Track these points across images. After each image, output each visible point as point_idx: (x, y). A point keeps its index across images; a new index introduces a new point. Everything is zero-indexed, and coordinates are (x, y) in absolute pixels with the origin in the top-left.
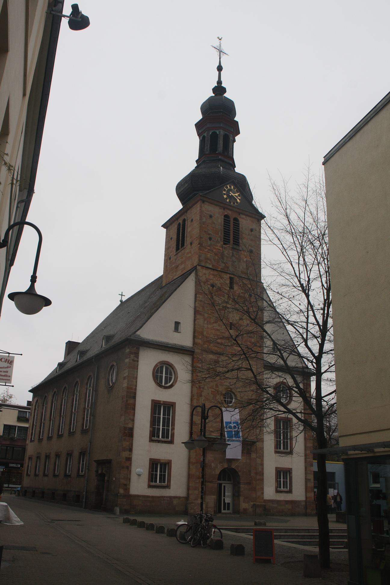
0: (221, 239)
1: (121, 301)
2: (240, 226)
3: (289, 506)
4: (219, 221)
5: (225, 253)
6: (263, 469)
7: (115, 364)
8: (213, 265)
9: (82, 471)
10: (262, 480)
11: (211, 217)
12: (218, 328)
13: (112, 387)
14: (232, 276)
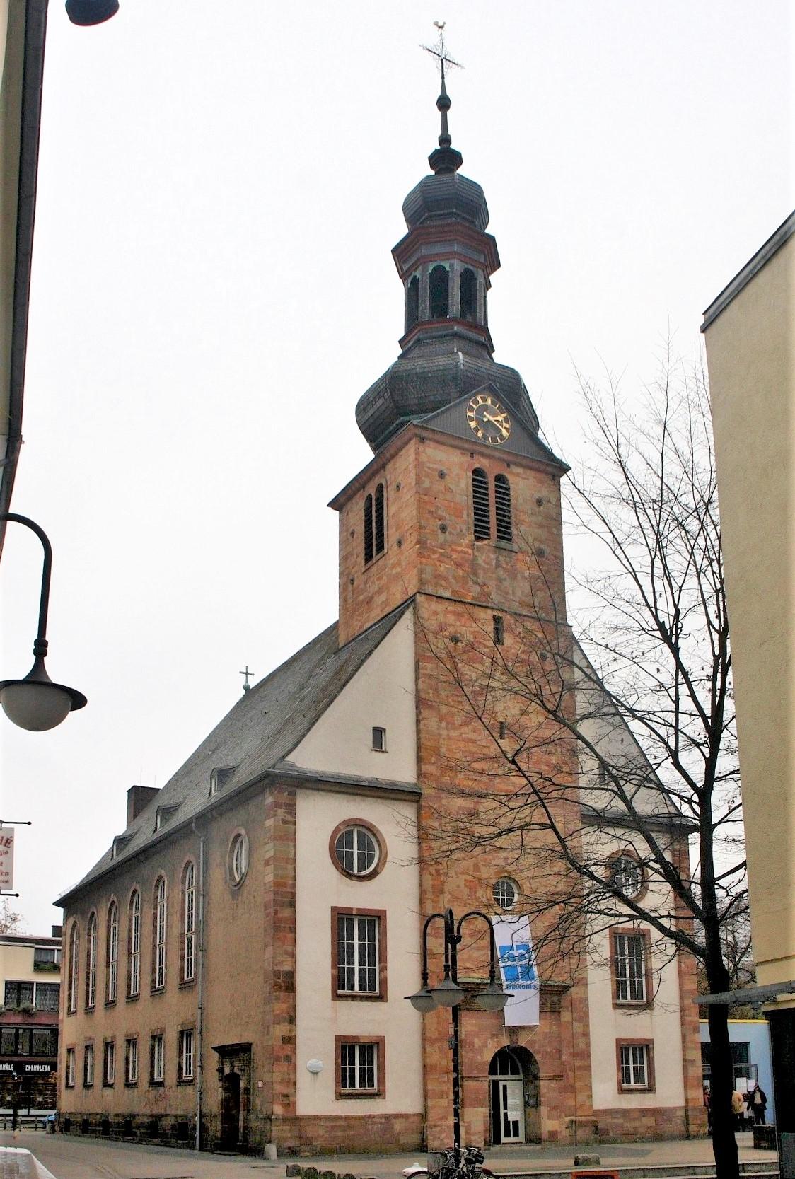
1: (246, 688)
3: (650, 1121)
4: (463, 485)
5: (480, 561)
6: (588, 1044)
7: (243, 832)
8: (453, 592)
9: (188, 1072)
10: (588, 1068)
11: (442, 475)
12: (473, 736)
13: (239, 885)
14: (499, 614)
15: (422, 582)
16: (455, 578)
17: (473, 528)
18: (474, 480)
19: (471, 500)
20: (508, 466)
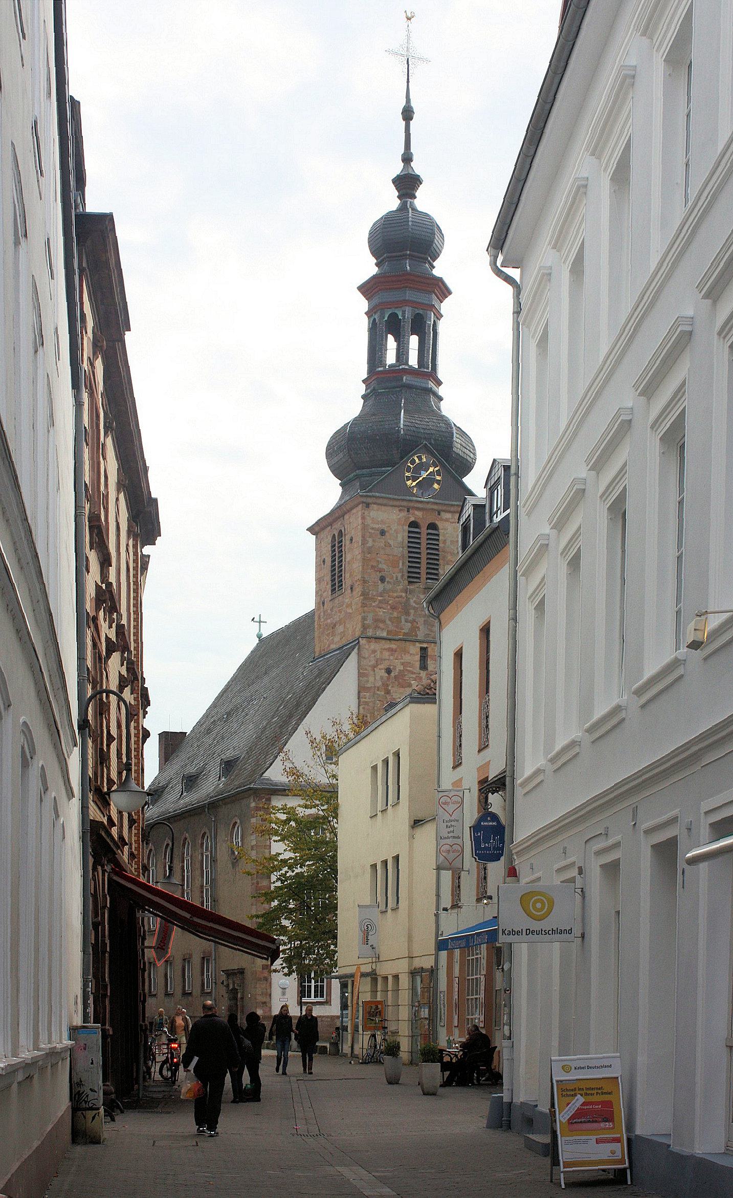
0: (403, 576)
1: (259, 636)
2: (441, 538)
4: (400, 539)
8: (389, 632)
11: (383, 533)
14: (425, 645)
15: (365, 627)
16: (390, 619)
17: (406, 575)
18: (409, 532)
19: (406, 550)
20: (439, 514)
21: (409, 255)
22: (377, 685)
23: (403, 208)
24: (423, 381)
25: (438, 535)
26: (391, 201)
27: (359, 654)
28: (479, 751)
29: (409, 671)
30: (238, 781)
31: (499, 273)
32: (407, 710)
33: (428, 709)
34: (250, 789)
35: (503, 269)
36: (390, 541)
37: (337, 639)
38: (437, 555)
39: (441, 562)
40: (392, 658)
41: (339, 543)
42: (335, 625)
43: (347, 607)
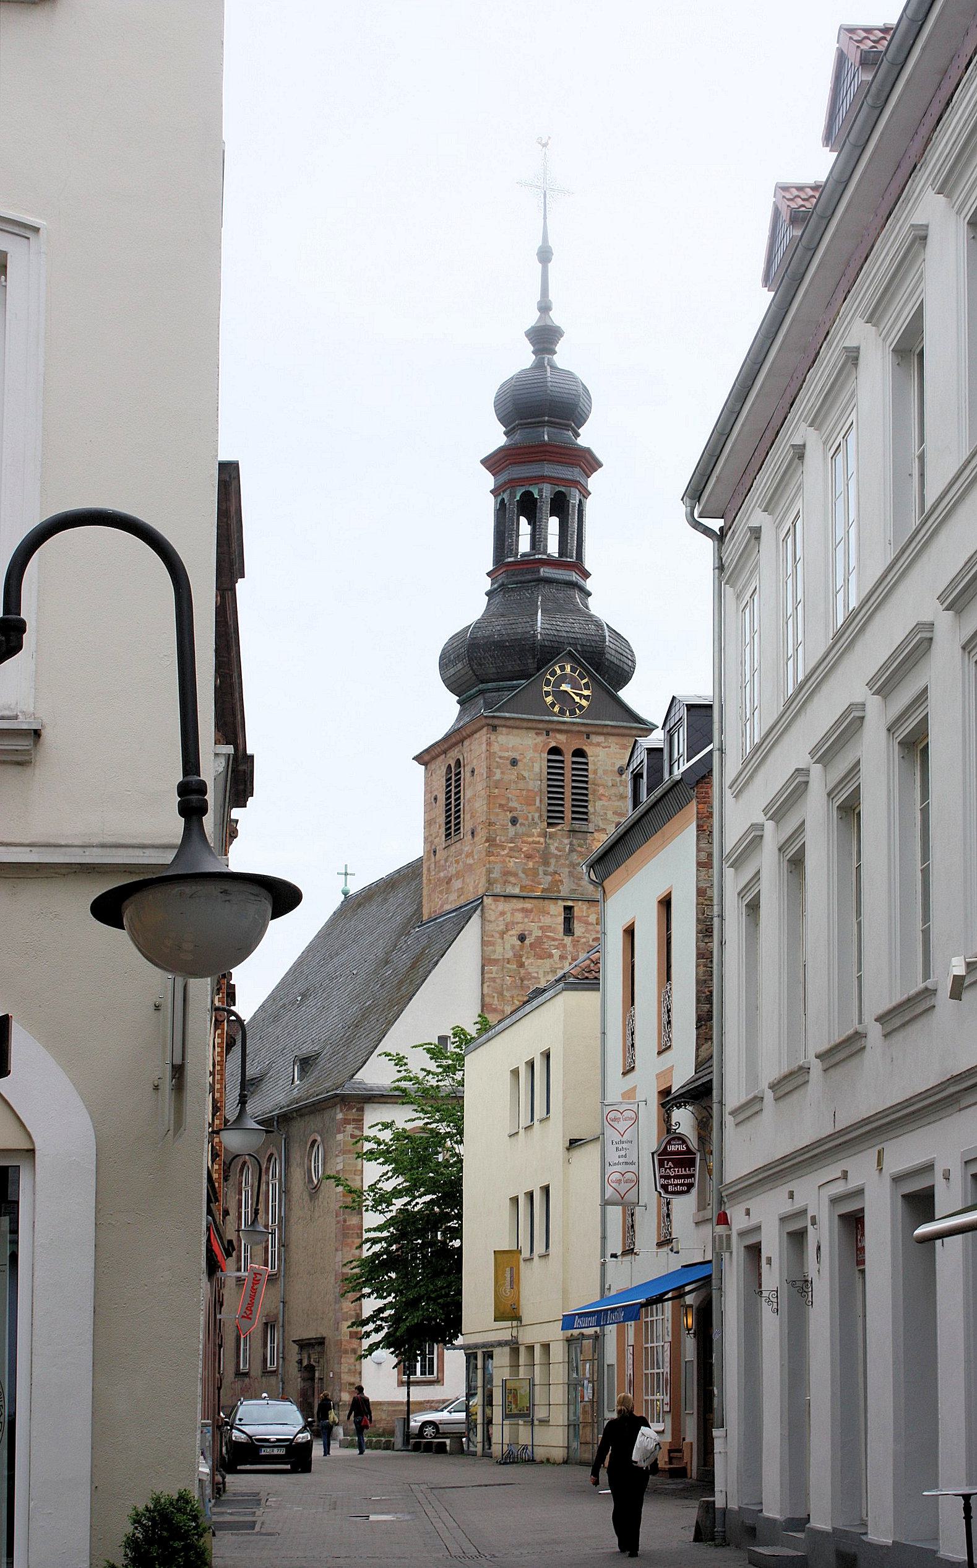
0: (541, 816)
1: (345, 893)
2: (591, 767)
4: (537, 769)
7: (319, 1139)
8: (522, 888)
11: (514, 763)
14: (570, 903)
15: (490, 882)
17: (545, 814)
18: (549, 761)
20: (588, 738)
21: (548, 422)
22: (507, 956)
23: (539, 366)
24: (568, 572)
25: (587, 764)
26: (524, 358)
27: (482, 916)
28: (659, 1053)
29: (548, 937)
30: (320, 1084)
31: (696, 525)
32: (560, 999)
33: (587, 999)
34: (337, 1095)
35: (701, 520)
36: (523, 773)
37: (453, 896)
38: (586, 789)
39: (590, 797)
40: (526, 920)
41: (456, 775)
42: (450, 879)
43: (467, 856)
